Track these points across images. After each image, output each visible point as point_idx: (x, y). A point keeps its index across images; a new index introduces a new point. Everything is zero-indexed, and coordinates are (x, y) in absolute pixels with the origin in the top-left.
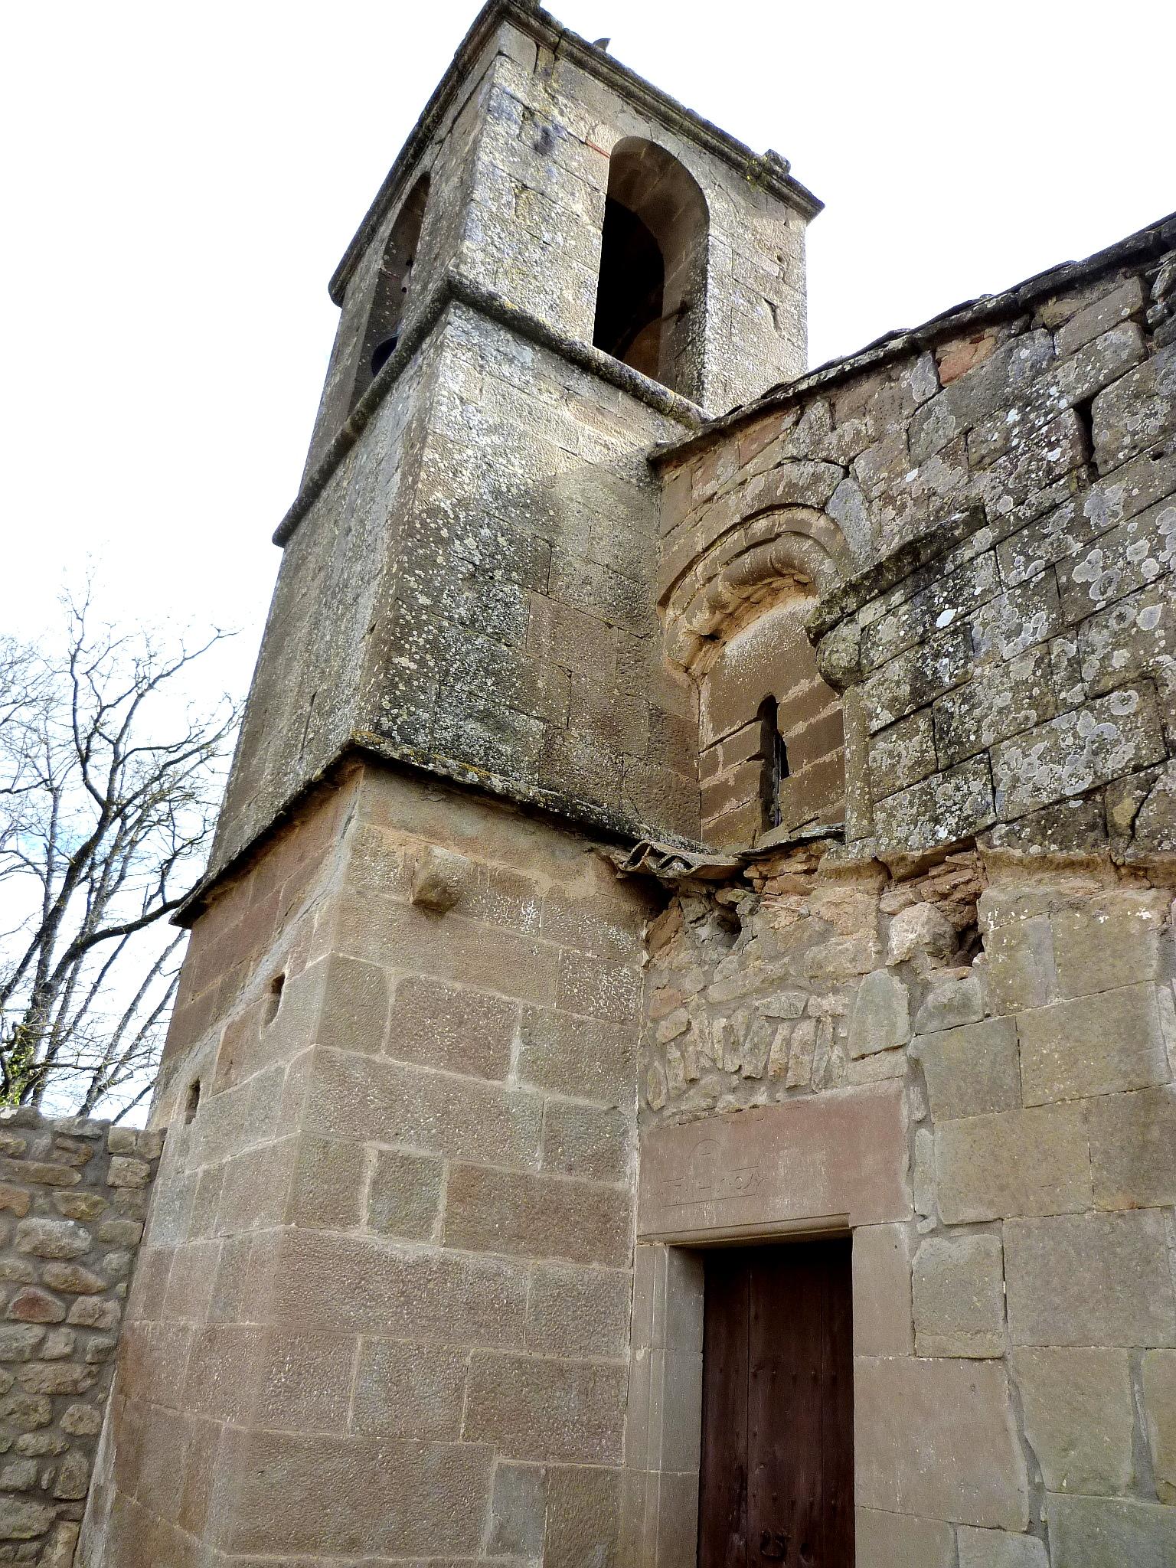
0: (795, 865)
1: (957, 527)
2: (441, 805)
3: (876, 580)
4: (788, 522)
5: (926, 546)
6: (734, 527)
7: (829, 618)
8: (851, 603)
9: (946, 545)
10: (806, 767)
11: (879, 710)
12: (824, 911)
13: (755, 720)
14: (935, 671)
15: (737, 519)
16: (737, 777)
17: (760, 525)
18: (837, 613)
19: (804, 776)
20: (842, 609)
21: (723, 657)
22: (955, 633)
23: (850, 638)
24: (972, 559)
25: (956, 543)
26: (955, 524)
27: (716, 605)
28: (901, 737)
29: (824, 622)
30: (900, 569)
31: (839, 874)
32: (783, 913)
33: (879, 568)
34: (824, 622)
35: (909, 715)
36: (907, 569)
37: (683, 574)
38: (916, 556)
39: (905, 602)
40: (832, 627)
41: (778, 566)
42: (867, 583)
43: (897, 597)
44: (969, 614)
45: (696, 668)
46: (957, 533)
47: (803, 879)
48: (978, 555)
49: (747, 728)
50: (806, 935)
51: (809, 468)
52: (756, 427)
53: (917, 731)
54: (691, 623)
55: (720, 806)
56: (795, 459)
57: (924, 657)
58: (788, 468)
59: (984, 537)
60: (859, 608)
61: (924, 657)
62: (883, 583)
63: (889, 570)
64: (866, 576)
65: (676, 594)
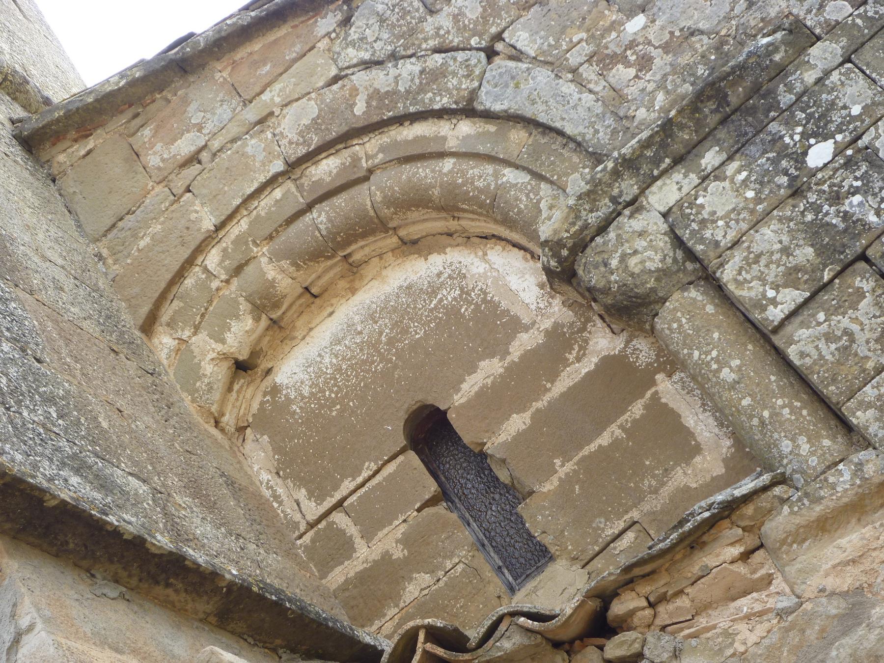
0: (724, 551)
1: (776, 50)
2: (122, 606)
3: (663, 145)
4: (382, 149)
5: (734, 84)
6: (272, 181)
7: (593, 219)
8: (628, 187)
9: (765, 76)
10: (564, 469)
11: (771, 293)
12: (831, 583)
13: (402, 451)
14: (846, 216)
15: (278, 166)
16: (406, 541)
17: (327, 168)
18: (605, 207)
19: (567, 482)
20: (614, 200)
21: (275, 390)
22: (849, 164)
23: (652, 228)
24: (819, 81)
25: (781, 71)
26: (772, 49)
27: (265, 303)
28: (839, 310)
29: (586, 226)
30: (699, 124)
31: (825, 526)
32: (742, 627)
33: (667, 127)
34: (586, 226)
35: (831, 281)
36: (712, 120)
37: (180, 275)
38: (722, 99)
39: (730, 158)
40: (602, 229)
41: (386, 212)
42: (649, 153)
43: (711, 158)
44: (859, 137)
45: (228, 419)
46: (777, 57)
47: (741, 568)
48: (827, 73)
49: (391, 468)
50: (812, 634)
51: (409, 69)
52: (256, 46)
53: (860, 294)
54: (223, 341)
55: (394, 597)
56: (367, 65)
57: (816, 209)
58: (360, 78)
59: (823, 54)
60: (642, 191)
61: (816, 209)
62: (677, 148)
63: (682, 127)
64: (646, 144)
65: (167, 313)
